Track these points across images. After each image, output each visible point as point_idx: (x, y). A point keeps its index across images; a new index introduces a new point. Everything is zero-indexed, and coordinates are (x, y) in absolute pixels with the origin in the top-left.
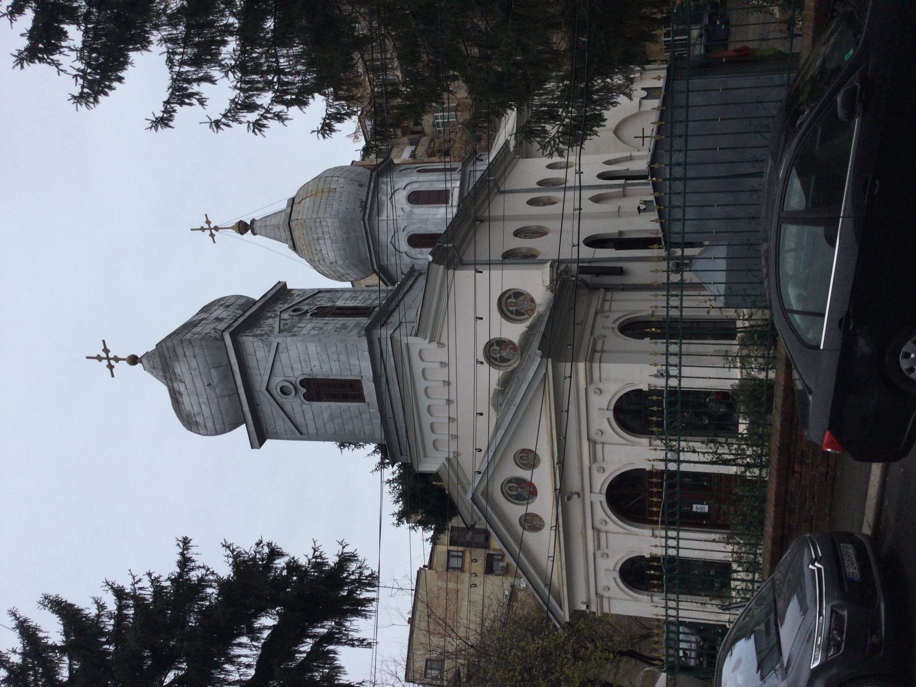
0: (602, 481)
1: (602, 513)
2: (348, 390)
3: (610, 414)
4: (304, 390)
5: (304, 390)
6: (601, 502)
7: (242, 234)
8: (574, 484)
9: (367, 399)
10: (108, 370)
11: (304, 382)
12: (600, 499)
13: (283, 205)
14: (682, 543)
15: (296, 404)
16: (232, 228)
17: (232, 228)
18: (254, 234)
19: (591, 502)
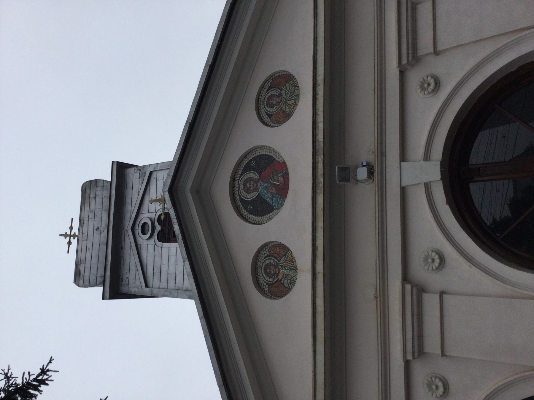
0: (431, 116)
1: (435, 227)
6: (427, 186)
8: (362, 142)
10: (67, 246)
12: (425, 172)
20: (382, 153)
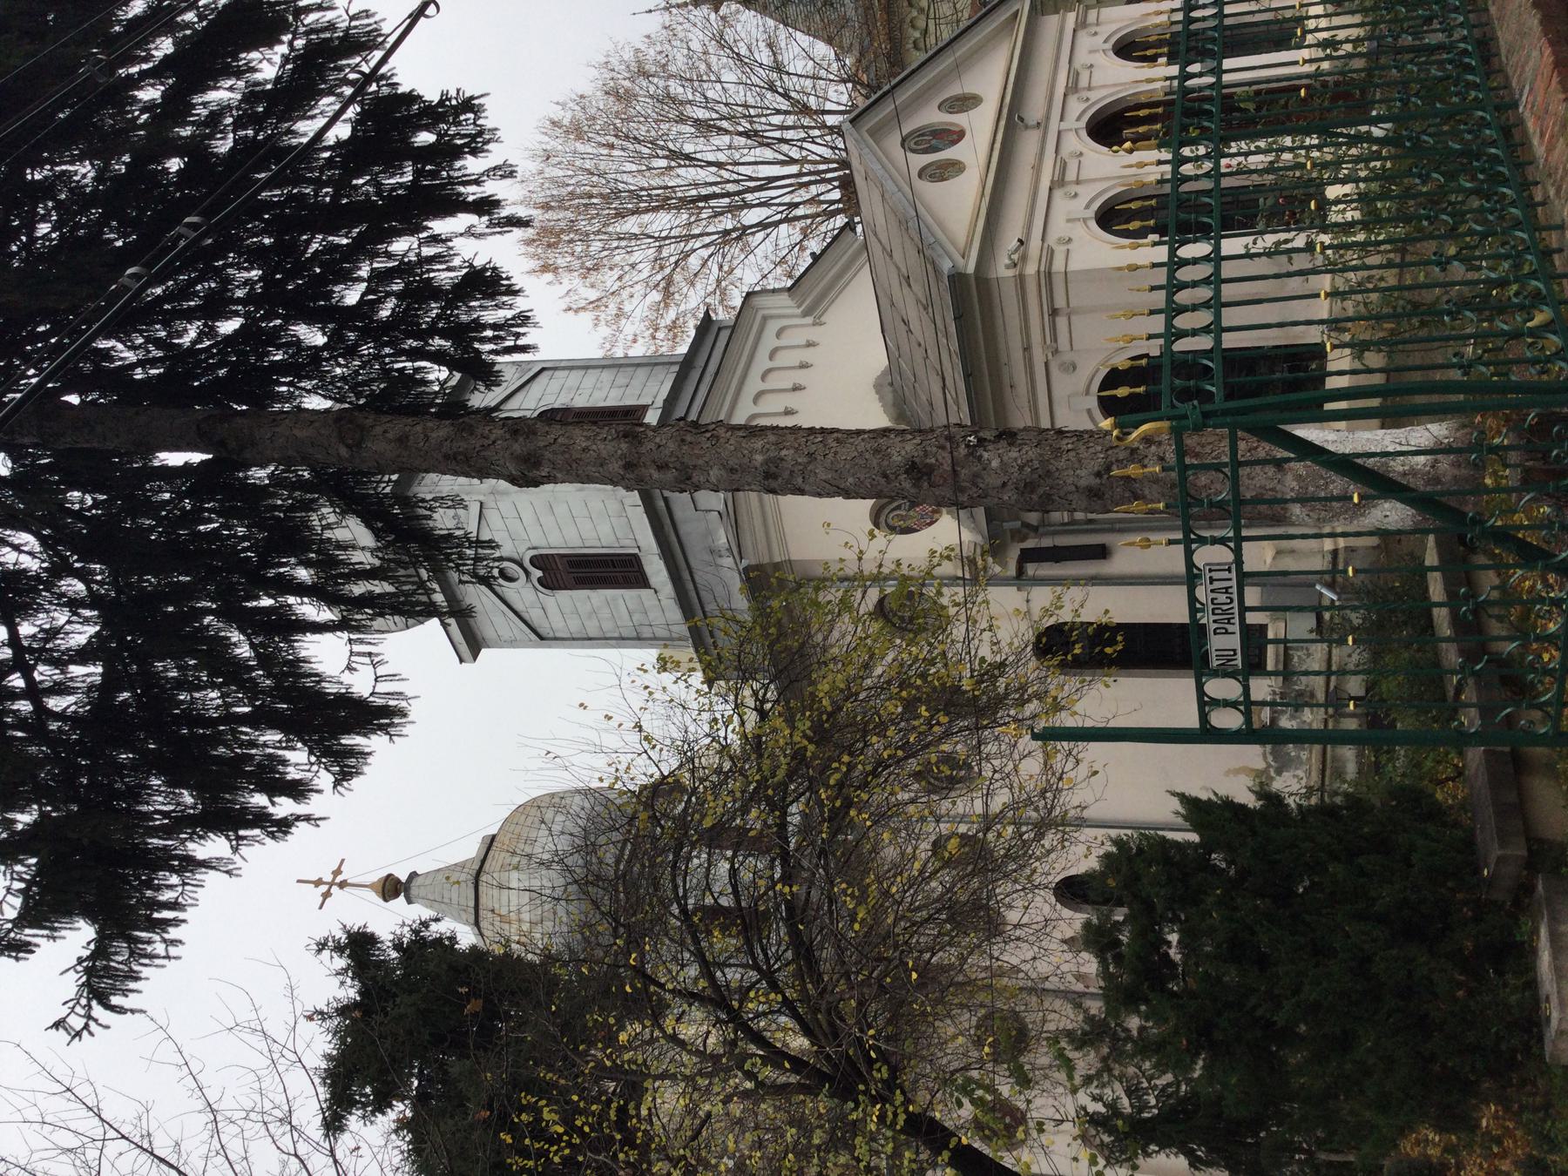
2: (616, 570)
4: (539, 573)
7: (386, 900)
8: (1035, 108)
9: (653, 581)
11: (537, 561)
13: (470, 850)
14: (1230, 317)
15: (523, 592)
16: (371, 886)
17: (371, 886)
18: (409, 902)
19: (1059, 132)
20: (1048, 118)
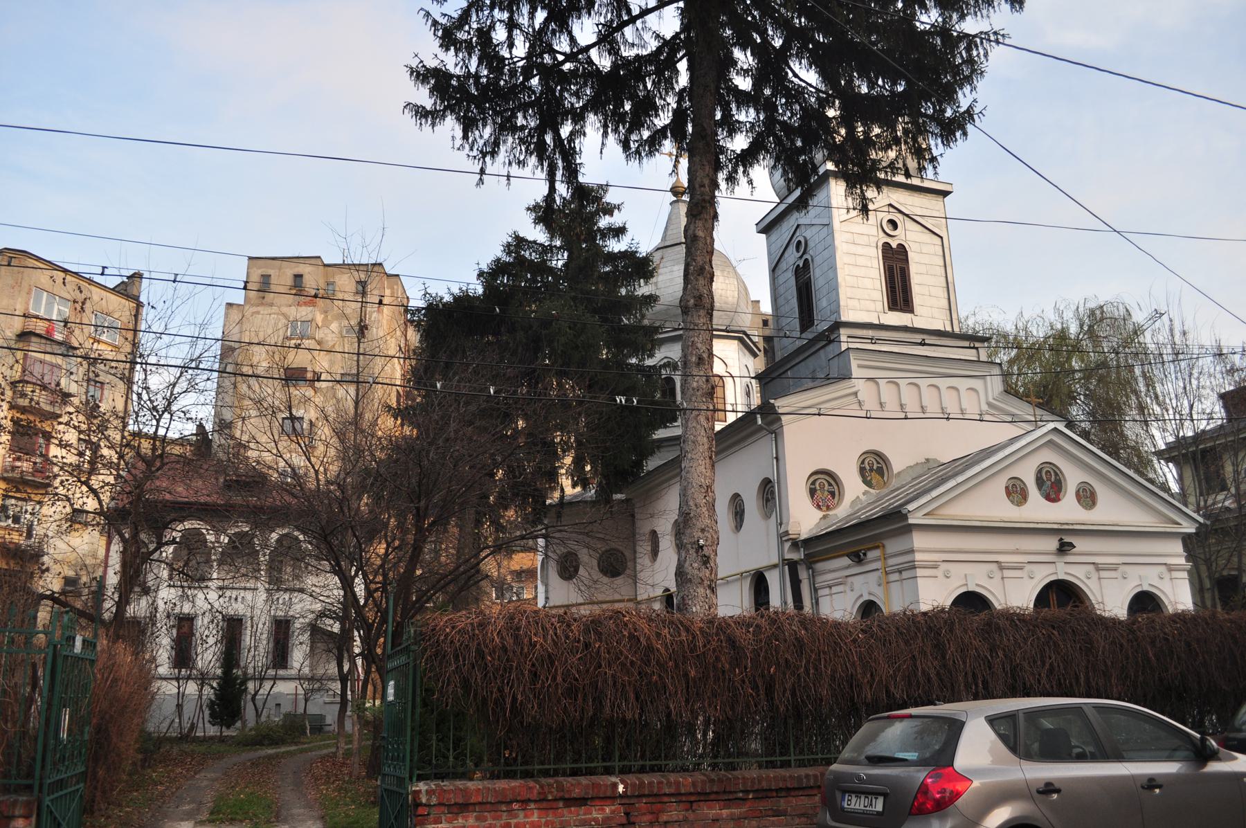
3: (972, 588)
5: (894, 245)
12: (1062, 571)
